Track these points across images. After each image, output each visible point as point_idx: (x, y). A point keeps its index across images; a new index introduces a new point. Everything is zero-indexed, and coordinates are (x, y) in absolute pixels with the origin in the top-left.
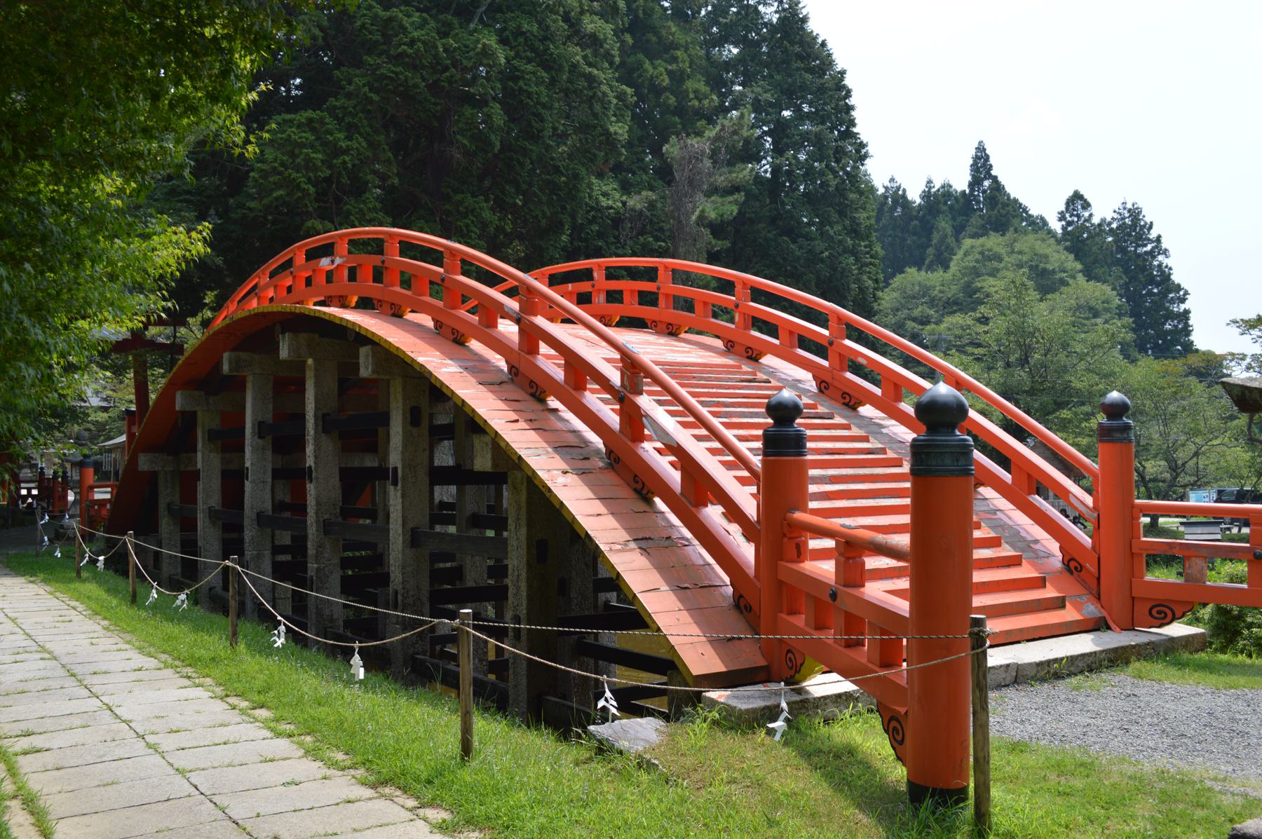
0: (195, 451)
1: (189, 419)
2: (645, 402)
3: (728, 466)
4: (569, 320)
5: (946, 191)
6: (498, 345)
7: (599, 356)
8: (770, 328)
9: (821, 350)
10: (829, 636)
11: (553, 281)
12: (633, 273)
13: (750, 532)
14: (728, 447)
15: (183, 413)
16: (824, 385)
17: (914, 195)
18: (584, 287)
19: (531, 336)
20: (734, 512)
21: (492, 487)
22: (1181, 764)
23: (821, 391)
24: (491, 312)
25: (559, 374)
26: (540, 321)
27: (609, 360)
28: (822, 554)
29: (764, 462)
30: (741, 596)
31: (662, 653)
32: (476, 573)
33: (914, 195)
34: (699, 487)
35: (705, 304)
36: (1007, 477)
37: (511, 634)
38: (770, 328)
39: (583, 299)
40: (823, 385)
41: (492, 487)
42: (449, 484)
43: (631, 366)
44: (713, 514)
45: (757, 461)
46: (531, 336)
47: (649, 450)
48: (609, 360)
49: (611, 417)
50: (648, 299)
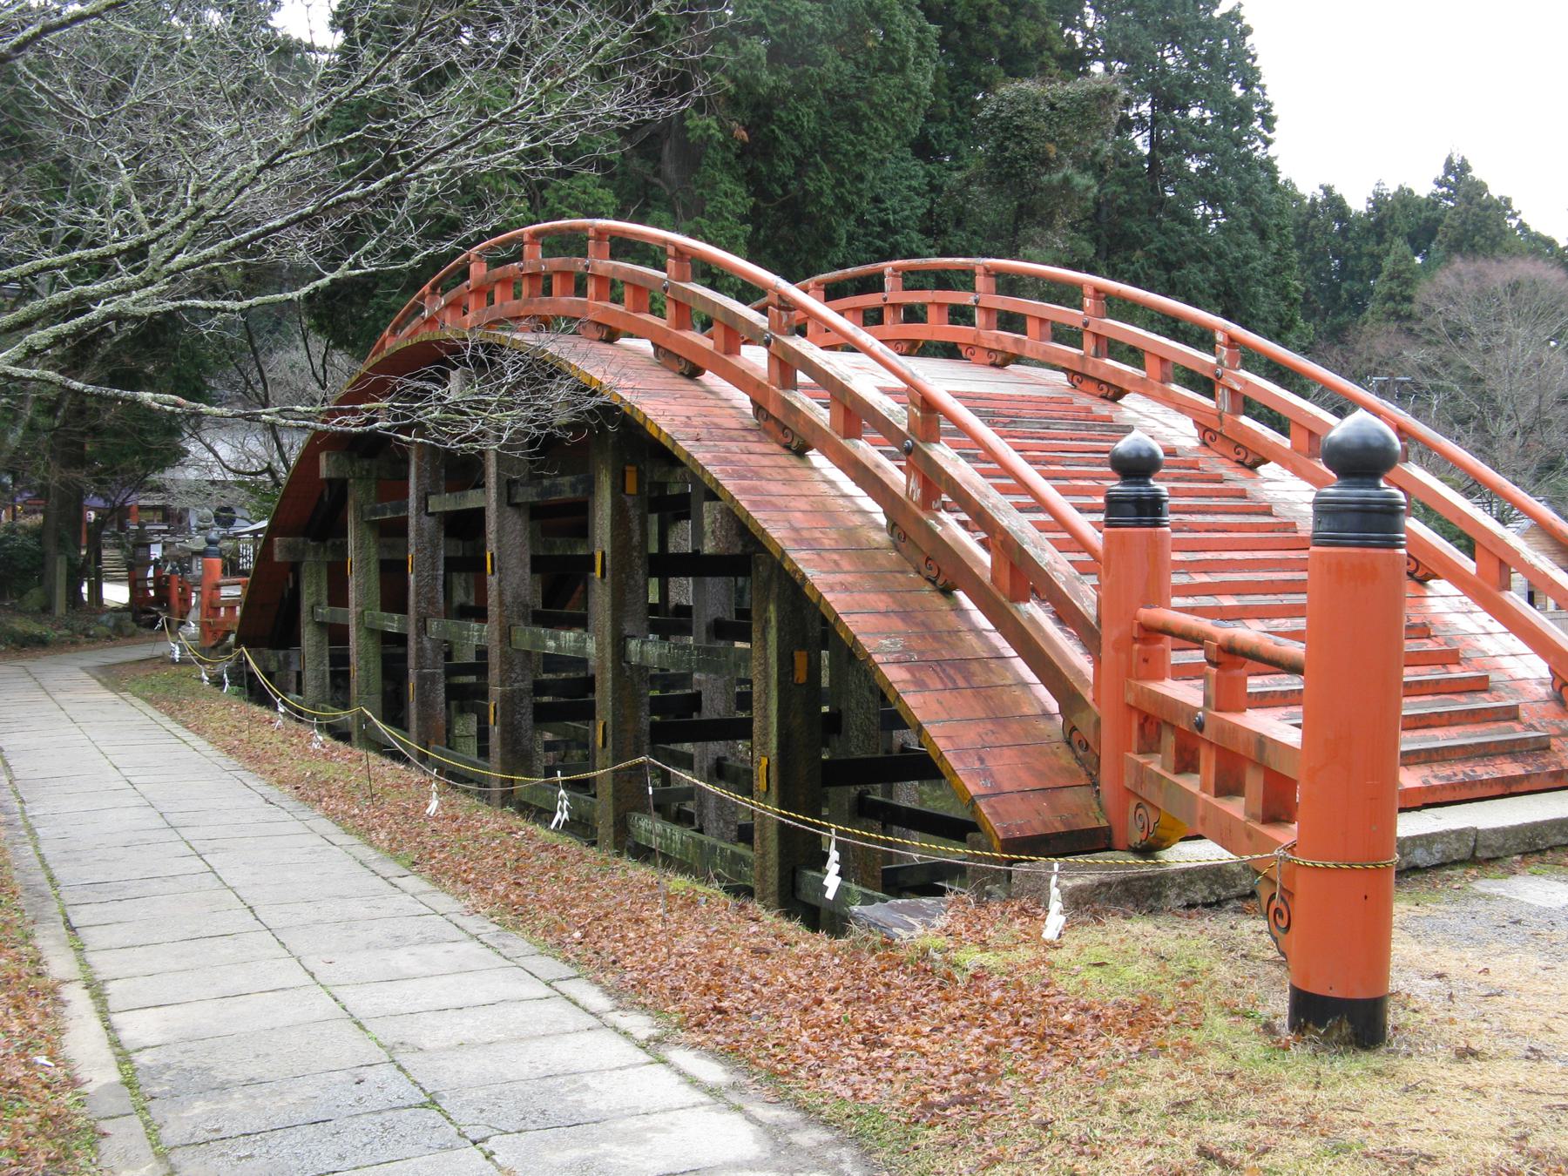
0: (344, 533)
1: (338, 489)
2: (943, 454)
3: (1061, 547)
4: (852, 347)
5: (1405, 199)
6: (741, 379)
7: (866, 378)
8: (1134, 355)
9: (1206, 385)
10: (1235, 808)
11: (832, 293)
12: (943, 280)
13: (1089, 636)
14: (1061, 523)
15: (329, 481)
16: (1209, 433)
17: (1358, 203)
18: (871, 300)
19: (787, 365)
20: (1066, 614)
21: (672, 550)
22: (122, 27)
23: (1204, 444)
24: (735, 334)
25: (823, 417)
26: (799, 344)
27: (885, 391)
28: (1184, 673)
29: (1108, 540)
30: (1074, 729)
31: (959, 813)
32: (715, 707)
33: (1358, 203)
34: (1021, 575)
35: (1042, 321)
36: (1470, 566)
37: (996, 843)
38: (1134, 355)
39: (872, 318)
40: (1208, 434)
41: (672, 550)
42: (686, 575)
43: (928, 408)
44: (1036, 612)
45: (1095, 538)
46: (787, 365)
47: (951, 526)
48: (885, 391)
49: (896, 476)
50: (961, 315)
